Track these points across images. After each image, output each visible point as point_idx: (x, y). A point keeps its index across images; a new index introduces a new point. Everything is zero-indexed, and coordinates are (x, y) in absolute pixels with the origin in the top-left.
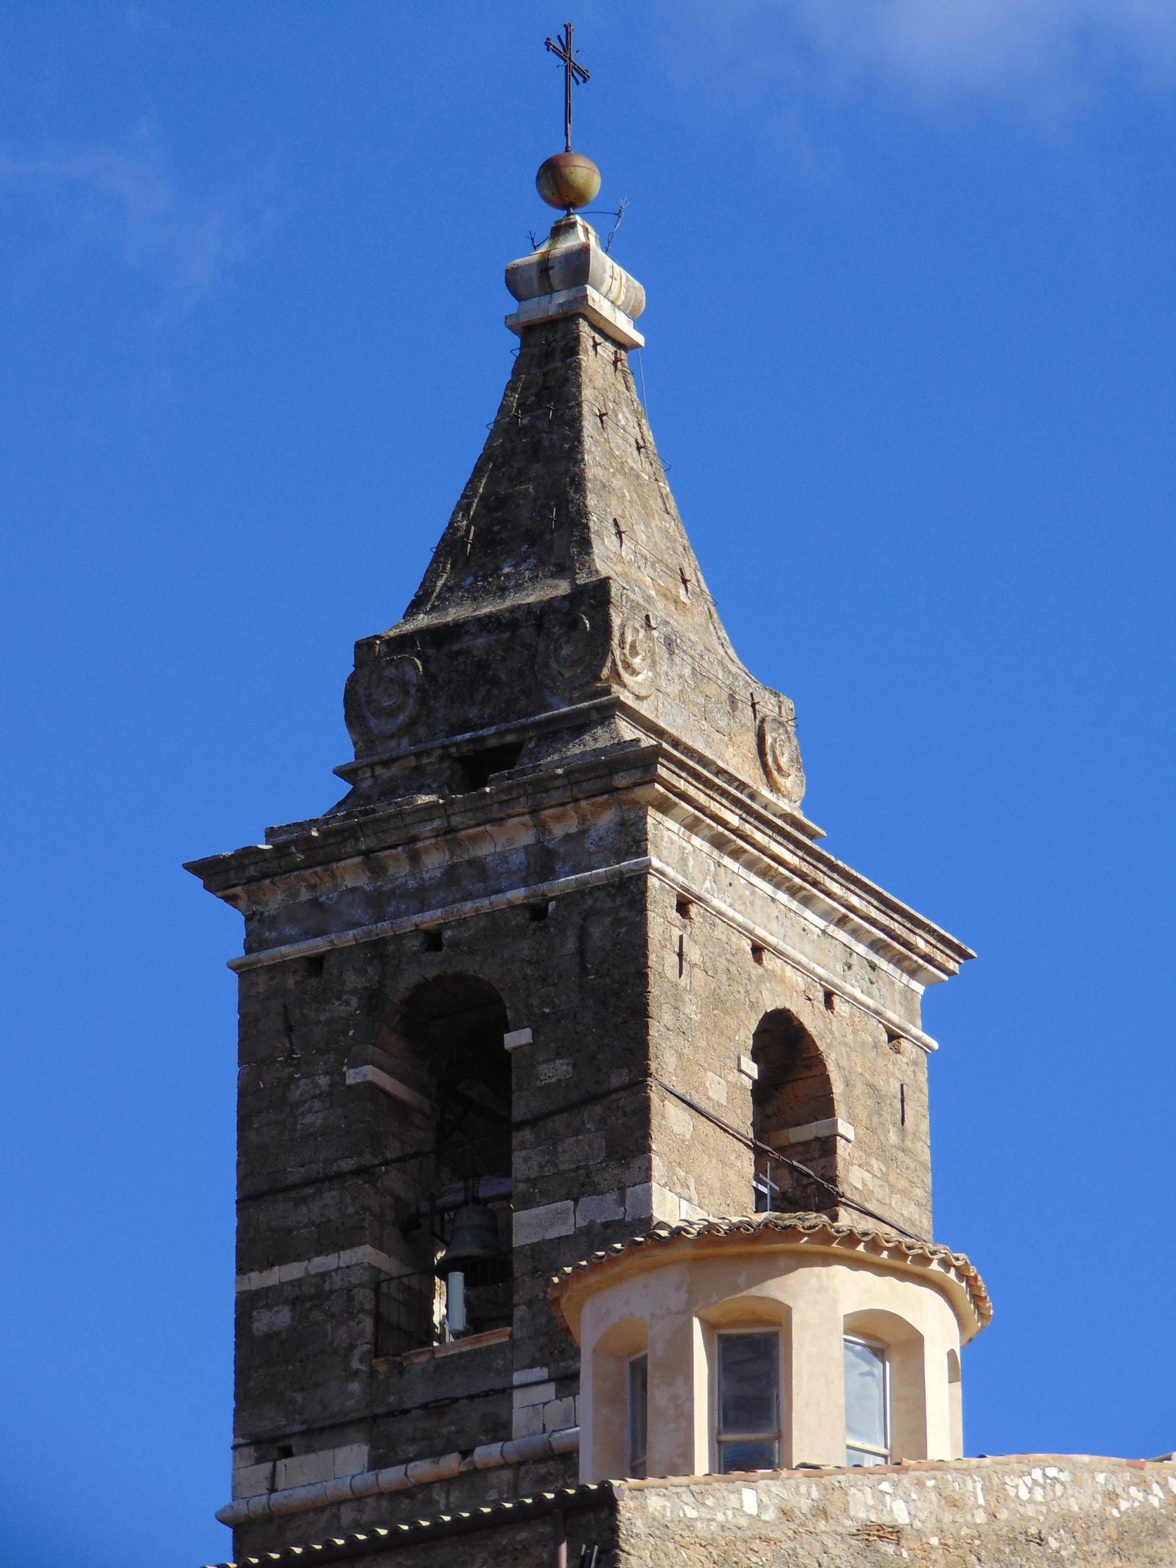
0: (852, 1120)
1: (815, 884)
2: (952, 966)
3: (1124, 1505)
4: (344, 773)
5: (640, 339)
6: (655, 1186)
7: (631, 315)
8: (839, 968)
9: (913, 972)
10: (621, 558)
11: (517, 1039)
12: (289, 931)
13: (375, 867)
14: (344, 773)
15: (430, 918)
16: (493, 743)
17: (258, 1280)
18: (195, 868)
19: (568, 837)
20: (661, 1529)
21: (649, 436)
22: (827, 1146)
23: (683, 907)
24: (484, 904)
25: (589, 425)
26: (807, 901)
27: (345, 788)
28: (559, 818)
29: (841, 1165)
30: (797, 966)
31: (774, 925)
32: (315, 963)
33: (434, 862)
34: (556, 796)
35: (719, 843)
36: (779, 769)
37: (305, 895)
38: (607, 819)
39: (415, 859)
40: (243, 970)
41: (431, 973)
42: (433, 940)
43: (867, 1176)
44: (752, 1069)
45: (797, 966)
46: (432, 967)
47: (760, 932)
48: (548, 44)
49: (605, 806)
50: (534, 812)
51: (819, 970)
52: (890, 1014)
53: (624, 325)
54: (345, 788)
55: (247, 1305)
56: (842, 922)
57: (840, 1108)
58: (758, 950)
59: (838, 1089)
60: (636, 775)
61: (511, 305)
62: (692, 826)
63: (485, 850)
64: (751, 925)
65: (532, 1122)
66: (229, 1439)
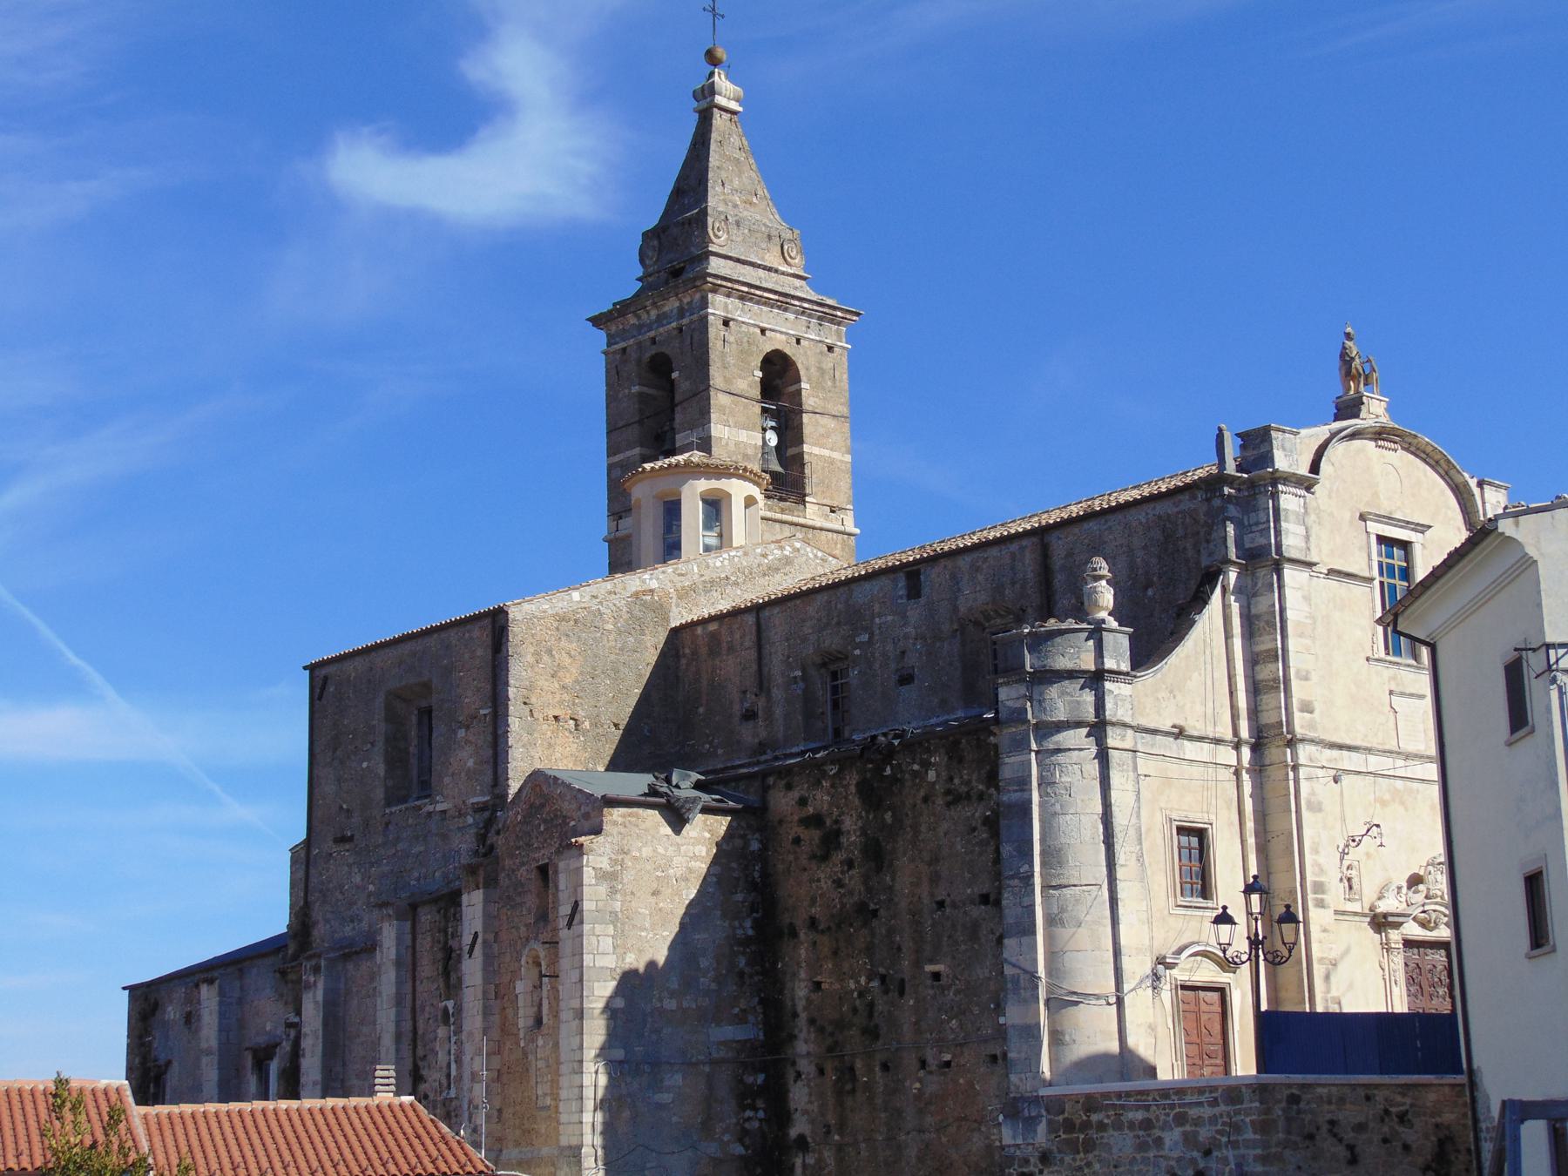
0: (809, 381)
1: (787, 303)
2: (854, 318)
3: (770, 558)
4: (639, 279)
5: (740, 109)
6: (712, 425)
7: (737, 101)
8: (804, 329)
9: (839, 324)
10: (724, 194)
11: (675, 375)
12: (617, 339)
13: (639, 317)
14: (639, 279)
15: (652, 334)
16: (678, 267)
17: (617, 458)
18: (588, 320)
19: (688, 303)
20: (530, 620)
21: (746, 143)
22: (799, 392)
23: (726, 323)
24: (666, 328)
25: (713, 147)
26: (786, 310)
27: (640, 284)
28: (685, 297)
29: (804, 399)
30: (781, 332)
31: (772, 320)
32: (624, 350)
33: (654, 313)
34: (681, 290)
35: (742, 298)
36: (791, 257)
37: (621, 327)
38: (698, 296)
39: (648, 312)
40: (606, 353)
41: (653, 352)
42: (653, 340)
43: (817, 400)
44: (760, 374)
45: (781, 332)
46: (653, 351)
47: (761, 325)
48: (704, 9)
49: (697, 291)
50: (677, 295)
51: (792, 332)
52: (827, 341)
53: (734, 106)
54: (640, 284)
55: (610, 468)
56: (803, 313)
57: (803, 378)
58: (763, 331)
59: (802, 373)
60: (702, 282)
61: (695, 104)
62: (728, 296)
63: (666, 309)
64: (757, 323)
65: (681, 403)
66: (606, 513)
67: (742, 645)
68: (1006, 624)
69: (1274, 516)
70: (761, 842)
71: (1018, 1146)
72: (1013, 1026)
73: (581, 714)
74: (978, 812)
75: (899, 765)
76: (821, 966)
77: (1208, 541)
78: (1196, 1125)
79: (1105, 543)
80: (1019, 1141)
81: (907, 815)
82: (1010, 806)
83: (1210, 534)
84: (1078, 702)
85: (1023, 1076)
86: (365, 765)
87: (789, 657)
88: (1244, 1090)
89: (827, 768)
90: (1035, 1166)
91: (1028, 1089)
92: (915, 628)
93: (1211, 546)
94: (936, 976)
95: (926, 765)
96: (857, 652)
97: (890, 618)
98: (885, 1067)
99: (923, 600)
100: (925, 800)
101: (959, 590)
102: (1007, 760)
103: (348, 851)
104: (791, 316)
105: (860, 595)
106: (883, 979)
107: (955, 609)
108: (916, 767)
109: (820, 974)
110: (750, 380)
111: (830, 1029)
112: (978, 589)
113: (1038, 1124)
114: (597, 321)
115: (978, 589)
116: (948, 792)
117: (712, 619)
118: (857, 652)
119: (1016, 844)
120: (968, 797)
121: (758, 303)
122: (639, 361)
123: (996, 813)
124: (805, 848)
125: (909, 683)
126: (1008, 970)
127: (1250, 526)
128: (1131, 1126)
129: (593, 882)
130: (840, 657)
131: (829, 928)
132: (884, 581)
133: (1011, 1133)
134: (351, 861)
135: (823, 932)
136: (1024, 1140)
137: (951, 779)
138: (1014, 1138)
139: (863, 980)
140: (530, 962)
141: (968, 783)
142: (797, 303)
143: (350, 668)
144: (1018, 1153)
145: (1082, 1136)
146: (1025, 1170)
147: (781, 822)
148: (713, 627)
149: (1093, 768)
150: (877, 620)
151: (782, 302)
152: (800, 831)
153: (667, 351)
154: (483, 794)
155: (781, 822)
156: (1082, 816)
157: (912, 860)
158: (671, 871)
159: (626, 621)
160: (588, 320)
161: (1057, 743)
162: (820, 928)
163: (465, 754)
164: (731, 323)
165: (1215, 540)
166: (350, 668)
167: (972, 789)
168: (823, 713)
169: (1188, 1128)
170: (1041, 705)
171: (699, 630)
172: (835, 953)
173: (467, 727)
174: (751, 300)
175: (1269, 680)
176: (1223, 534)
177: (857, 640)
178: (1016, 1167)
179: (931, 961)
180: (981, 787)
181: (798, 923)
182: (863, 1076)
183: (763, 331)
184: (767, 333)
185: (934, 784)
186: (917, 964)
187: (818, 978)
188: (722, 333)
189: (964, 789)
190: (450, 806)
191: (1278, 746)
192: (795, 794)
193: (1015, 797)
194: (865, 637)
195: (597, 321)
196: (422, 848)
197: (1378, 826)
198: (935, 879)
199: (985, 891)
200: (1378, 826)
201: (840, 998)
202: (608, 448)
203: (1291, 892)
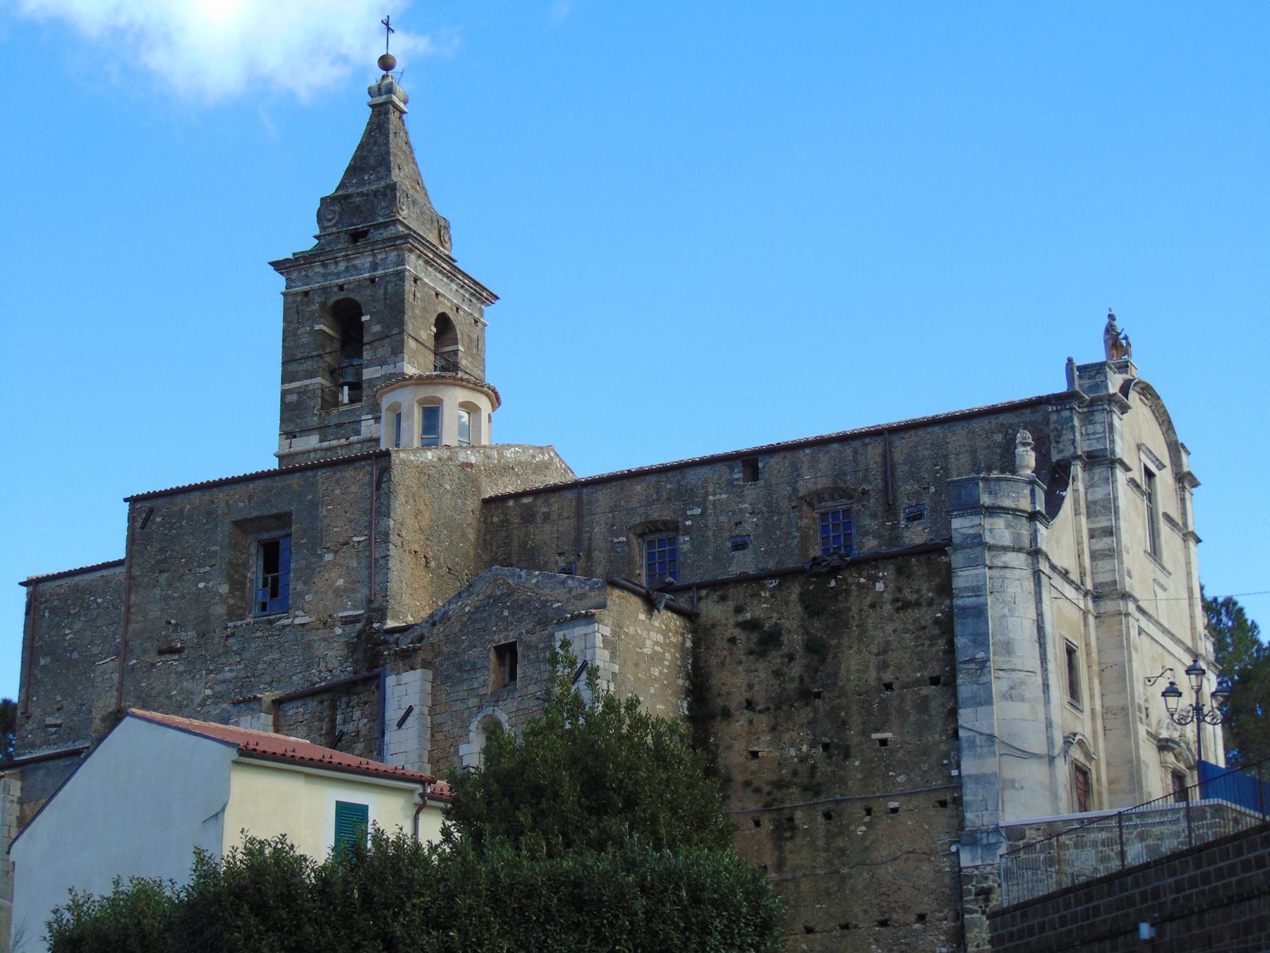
4: (316, 237)
11: (365, 318)
17: (287, 386)
18: (271, 264)
23: (415, 281)
26: (452, 281)
27: (316, 242)
30: (448, 300)
35: (427, 262)
40: (284, 294)
42: (341, 288)
44: (434, 329)
46: (341, 296)
54: (316, 242)
55: (284, 393)
56: (462, 287)
57: (460, 342)
58: (437, 294)
61: (369, 99)
65: (370, 343)
66: (278, 432)
67: (560, 515)
68: (836, 506)
69: (1109, 428)
70: (693, 642)
71: (977, 867)
72: (970, 776)
73: (430, 555)
74: (927, 616)
75: (845, 580)
76: (758, 738)
77: (1058, 442)
78: (1159, 839)
79: (948, 443)
80: (979, 862)
81: (853, 617)
82: (964, 609)
83: (1060, 436)
84: (1019, 534)
85: (979, 813)
86: (201, 585)
87: (613, 526)
88: (1208, 809)
89: (767, 582)
90: (994, 881)
91: (985, 823)
92: (751, 504)
93: (1061, 446)
94: (883, 742)
95: (875, 579)
96: (688, 523)
97: (724, 496)
98: (828, 816)
99: (761, 483)
100: (873, 606)
101: (799, 475)
102: (960, 573)
103: (175, 660)
104: (454, 286)
105: (692, 476)
106: (826, 747)
107: (795, 490)
108: (862, 580)
109: (758, 744)
110: (427, 332)
111: (767, 789)
112: (819, 474)
113: (998, 849)
114: (278, 266)
115: (819, 474)
116: (896, 600)
117: (525, 494)
118: (688, 523)
119: (970, 637)
120: (918, 604)
121: (436, 269)
122: (323, 305)
123: (950, 615)
124: (741, 646)
125: (744, 548)
126: (962, 733)
127: (1088, 435)
128: (1094, 844)
129: (602, 645)
130: (673, 527)
131: (767, 709)
132: (722, 468)
133: (969, 857)
134: (181, 668)
135: (761, 712)
136: (982, 861)
137: (900, 590)
138: (973, 860)
139: (805, 748)
140: (480, 728)
141: (918, 591)
142: (460, 277)
143: (187, 503)
144: (976, 872)
145: (1042, 856)
146: (985, 885)
147: (713, 626)
148: (526, 500)
149: (1029, 585)
150: (711, 498)
151: (451, 273)
152: (737, 632)
153: (358, 298)
154: (354, 607)
155: (713, 626)
156: (1024, 620)
157: (860, 652)
158: (645, 650)
159: (457, 485)
160: (271, 264)
161: (1004, 562)
162: (758, 708)
163: (333, 575)
164: (418, 282)
165: (1064, 441)
166: (187, 503)
167: (922, 596)
168: (639, 575)
169: (1150, 842)
170: (991, 533)
171: (511, 503)
172: (773, 729)
173: (336, 552)
174: (432, 266)
175: (1104, 550)
176: (1072, 437)
177: (689, 513)
178: (974, 883)
179: (877, 731)
180: (930, 595)
181: (733, 706)
182: (804, 824)
183: (437, 294)
184: (440, 297)
185: (882, 593)
186: (865, 733)
187: (755, 749)
188: (413, 289)
189: (914, 597)
190: (313, 619)
191: (1113, 599)
192: (731, 604)
193: (969, 601)
194: (698, 511)
195: (278, 266)
196: (276, 656)
197: (1171, 670)
198: (883, 666)
199: (935, 675)
200: (1171, 670)
201: (779, 764)
202: (282, 379)
203: (1123, 709)
